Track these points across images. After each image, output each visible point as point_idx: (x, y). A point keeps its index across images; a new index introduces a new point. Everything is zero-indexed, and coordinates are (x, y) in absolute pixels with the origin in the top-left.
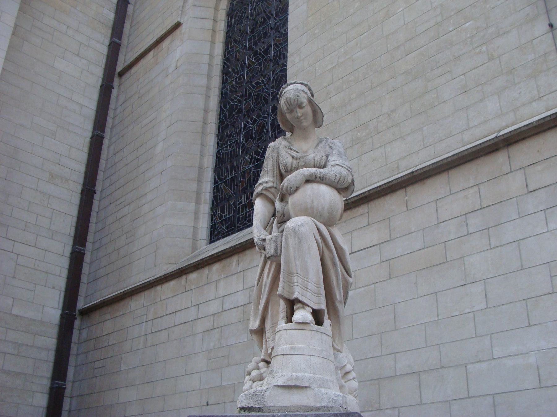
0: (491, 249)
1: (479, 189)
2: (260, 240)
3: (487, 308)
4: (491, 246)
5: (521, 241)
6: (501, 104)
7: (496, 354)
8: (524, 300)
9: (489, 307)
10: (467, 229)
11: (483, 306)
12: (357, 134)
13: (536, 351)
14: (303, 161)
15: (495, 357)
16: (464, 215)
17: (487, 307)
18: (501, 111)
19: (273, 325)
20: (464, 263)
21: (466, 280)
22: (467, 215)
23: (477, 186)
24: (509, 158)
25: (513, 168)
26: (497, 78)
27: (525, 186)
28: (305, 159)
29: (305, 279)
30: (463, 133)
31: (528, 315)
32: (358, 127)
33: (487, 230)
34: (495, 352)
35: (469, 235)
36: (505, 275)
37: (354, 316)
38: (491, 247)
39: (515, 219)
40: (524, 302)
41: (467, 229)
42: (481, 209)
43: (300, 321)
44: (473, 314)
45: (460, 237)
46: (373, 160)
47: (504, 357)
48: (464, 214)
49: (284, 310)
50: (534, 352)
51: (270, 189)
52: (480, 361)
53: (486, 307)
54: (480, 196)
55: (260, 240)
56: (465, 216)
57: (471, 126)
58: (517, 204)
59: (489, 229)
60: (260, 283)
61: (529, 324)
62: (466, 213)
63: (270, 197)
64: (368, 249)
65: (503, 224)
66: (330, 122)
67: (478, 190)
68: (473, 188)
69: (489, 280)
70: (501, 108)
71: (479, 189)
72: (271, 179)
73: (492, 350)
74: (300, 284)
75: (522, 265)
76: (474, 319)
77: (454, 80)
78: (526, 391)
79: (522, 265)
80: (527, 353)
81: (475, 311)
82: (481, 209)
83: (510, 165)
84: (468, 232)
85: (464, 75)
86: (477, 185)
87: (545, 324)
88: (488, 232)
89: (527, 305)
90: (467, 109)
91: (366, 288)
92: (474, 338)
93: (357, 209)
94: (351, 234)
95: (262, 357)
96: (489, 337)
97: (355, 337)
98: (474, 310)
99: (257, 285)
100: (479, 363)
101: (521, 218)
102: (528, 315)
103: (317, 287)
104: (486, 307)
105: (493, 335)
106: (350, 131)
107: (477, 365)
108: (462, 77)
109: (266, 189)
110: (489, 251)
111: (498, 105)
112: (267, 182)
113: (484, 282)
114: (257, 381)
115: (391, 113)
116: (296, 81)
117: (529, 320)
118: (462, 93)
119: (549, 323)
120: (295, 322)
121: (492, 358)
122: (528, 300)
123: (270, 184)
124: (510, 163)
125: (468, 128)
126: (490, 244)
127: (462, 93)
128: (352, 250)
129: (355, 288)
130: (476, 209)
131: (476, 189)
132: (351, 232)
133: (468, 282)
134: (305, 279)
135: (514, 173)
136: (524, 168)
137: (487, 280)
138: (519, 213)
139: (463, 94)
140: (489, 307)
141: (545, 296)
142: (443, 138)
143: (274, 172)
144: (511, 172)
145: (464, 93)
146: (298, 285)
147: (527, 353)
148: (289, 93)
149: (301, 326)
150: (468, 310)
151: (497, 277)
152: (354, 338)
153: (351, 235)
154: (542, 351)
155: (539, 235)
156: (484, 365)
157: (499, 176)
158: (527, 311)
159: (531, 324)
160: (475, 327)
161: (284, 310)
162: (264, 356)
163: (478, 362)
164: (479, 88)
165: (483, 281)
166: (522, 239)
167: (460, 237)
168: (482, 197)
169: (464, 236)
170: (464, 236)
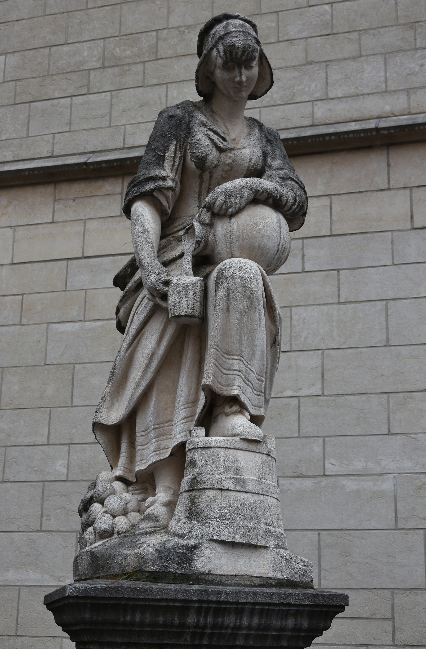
0: (339, 303)
1: (331, 203)
2: (160, 282)
3: (323, 395)
4: (340, 298)
5: (391, 303)
6: (388, 74)
7: (330, 469)
8: (385, 393)
9: (325, 393)
10: (303, 263)
11: (316, 390)
12: (114, 49)
13: (395, 473)
14: (230, 157)
15: (326, 474)
16: (300, 239)
17: (323, 392)
18: (386, 86)
19: (158, 426)
20: (291, 318)
21: (291, 345)
22: (305, 241)
23: (327, 197)
24: (389, 165)
25: (392, 183)
26: (387, 29)
27: (409, 217)
28: (234, 154)
29: (249, 366)
30: (315, 103)
31: (389, 417)
32: (118, 36)
33: (336, 272)
34: (328, 465)
35: (305, 274)
36: (359, 349)
37: (77, 367)
38: (341, 301)
39: (385, 266)
40: (385, 396)
41: (303, 263)
42: (330, 236)
43: (250, 438)
44: (297, 401)
45: (288, 273)
46: (142, 106)
47: (341, 475)
48: (301, 237)
49: (187, 406)
50: (392, 475)
51: (165, 192)
52: (302, 476)
53: (320, 393)
54: (331, 215)
55: (160, 282)
56: (301, 241)
57: (331, 95)
58: (392, 243)
59: (340, 271)
60: (131, 348)
61: (389, 431)
62: (304, 237)
63: (163, 203)
64: (116, 257)
65: (364, 268)
66: (62, 10)
67: (329, 204)
68: (320, 198)
69: (331, 351)
70: (386, 81)
71: (331, 203)
72: (171, 175)
73: (324, 461)
74: (242, 373)
75: (388, 339)
76: (299, 410)
77: (311, 8)
78: (373, 531)
79: (388, 339)
80: (381, 475)
81: (302, 396)
82: (330, 236)
83: (389, 178)
84: (303, 268)
85: (330, 5)
86: (328, 195)
87: (413, 436)
88: (338, 275)
89: (388, 402)
90: (327, 65)
91: (105, 322)
92: (296, 439)
93: (100, 183)
94: (85, 223)
95: (118, 472)
96: (321, 440)
97: (76, 402)
98: (300, 394)
99: (127, 351)
100: (301, 479)
101: (396, 267)
102: (389, 417)
103: (258, 380)
104: (320, 393)
105: (327, 439)
106: (101, 39)
107: (297, 482)
108: (327, 7)
109: (160, 189)
110: (336, 306)
111: (382, 74)
112: (164, 179)
113: (323, 353)
114: (119, 516)
115: (186, 31)
116: (239, 14)
117: (389, 425)
118: (322, 36)
119: (421, 435)
120: (241, 439)
121: (322, 474)
122: (391, 394)
123: (169, 183)
124: (388, 174)
125: (326, 99)
126: (339, 296)
127: (322, 36)
128: (83, 253)
129: (84, 319)
130: (321, 235)
131: (326, 201)
132: (85, 221)
133: (294, 348)
134: (249, 366)
135: (393, 192)
136: (411, 188)
137: (327, 351)
138: (393, 257)
139: (324, 37)
140: (325, 393)
141: (419, 393)
142: (279, 102)
143: (174, 162)
144: (389, 189)
145: (326, 37)
146: (239, 376)
147: (381, 475)
148: (237, 37)
149: (252, 447)
150: (289, 393)
151: (346, 350)
152: (73, 405)
153: (85, 226)
154: (404, 475)
155: (421, 299)
156: (308, 483)
157: (367, 191)
158: (389, 411)
159: (392, 432)
160: (299, 421)
161: (187, 406)
162: (123, 471)
163: (298, 477)
164: (354, 36)
165: (320, 352)
166: (394, 299)
167: (288, 273)
168: (334, 218)
169: (295, 273)
170: (295, 273)
